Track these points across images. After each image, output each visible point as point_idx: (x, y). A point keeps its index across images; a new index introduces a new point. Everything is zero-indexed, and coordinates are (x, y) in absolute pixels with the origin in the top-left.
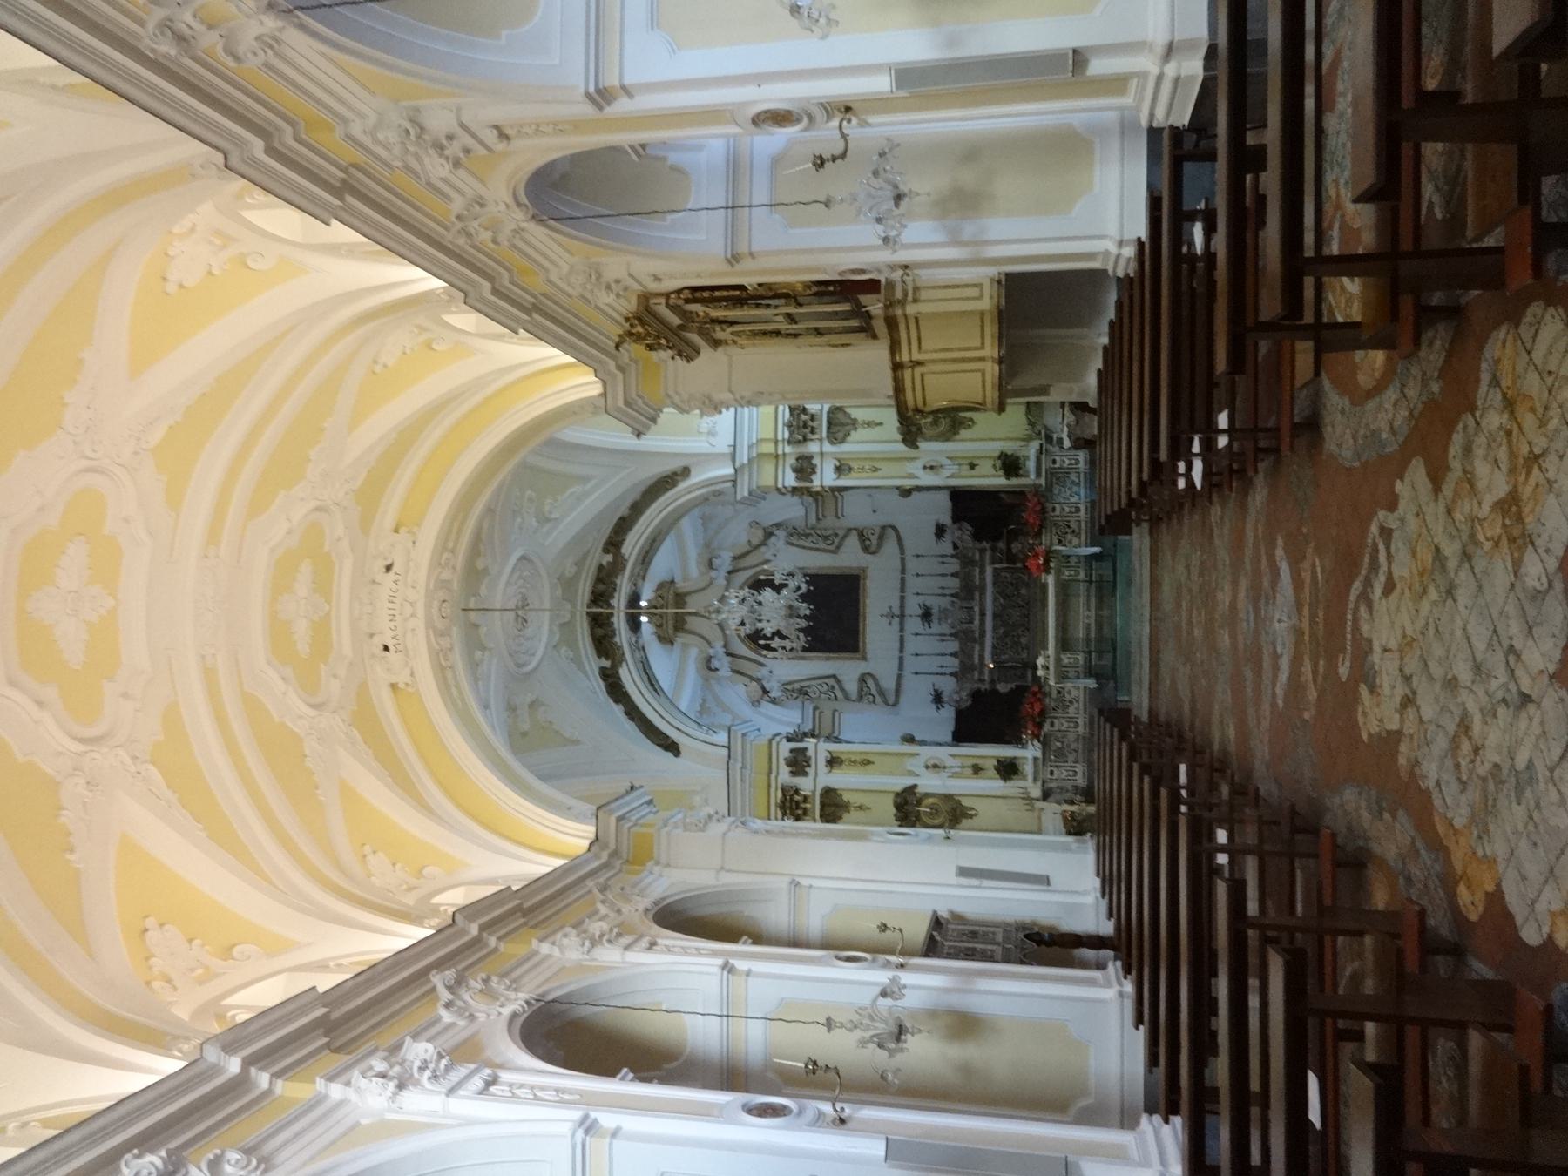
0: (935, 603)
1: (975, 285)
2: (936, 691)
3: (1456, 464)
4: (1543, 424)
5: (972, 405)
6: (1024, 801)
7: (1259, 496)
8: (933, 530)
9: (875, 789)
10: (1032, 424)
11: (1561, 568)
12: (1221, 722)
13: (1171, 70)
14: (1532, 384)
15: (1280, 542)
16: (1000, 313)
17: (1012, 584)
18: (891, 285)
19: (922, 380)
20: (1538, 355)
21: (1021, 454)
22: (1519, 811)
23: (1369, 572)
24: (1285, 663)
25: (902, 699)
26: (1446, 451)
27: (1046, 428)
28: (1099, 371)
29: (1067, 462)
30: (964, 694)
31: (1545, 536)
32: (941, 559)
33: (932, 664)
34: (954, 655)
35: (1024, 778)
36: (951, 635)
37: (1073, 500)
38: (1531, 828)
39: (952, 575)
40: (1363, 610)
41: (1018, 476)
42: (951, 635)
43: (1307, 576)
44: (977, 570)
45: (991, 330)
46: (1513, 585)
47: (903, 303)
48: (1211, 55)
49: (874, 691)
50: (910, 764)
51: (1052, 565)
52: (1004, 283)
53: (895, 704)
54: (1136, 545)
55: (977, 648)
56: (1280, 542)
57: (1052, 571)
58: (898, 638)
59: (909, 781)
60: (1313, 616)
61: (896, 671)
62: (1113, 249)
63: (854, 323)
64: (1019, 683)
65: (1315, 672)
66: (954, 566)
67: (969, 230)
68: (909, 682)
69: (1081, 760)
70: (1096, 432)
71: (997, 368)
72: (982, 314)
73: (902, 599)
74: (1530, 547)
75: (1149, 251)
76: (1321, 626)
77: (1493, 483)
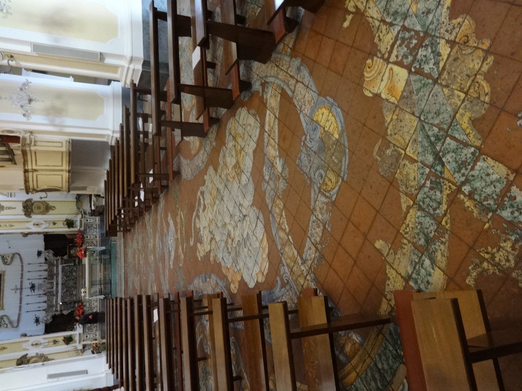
0: (36, 282)
1: (60, 142)
2: (36, 318)
3: (221, 162)
4: (243, 139)
5: (57, 188)
6: (75, 352)
7: (162, 203)
8: (37, 253)
9: (57, 141)
10: (78, 208)
11: (251, 174)
12: (151, 286)
13: (132, 66)
14: (240, 130)
15: (169, 214)
16: (69, 152)
17: (70, 272)
18: (24, 139)
19: (37, 177)
20: (240, 123)
21: (74, 219)
22: (246, 250)
23: (198, 207)
24: (173, 253)
25: (20, 324)
26: (218, 159)
27: (84, 210)
28: (105, 181)
29: (92, 220)
30: (49, 317)
31: (246, 168)
32: (40, 265)
33: (35, 307)
34: (45, 302)
35: (75, 342)
36: (43, 294)
37: (94, 233)
38: (249, 252)
39: (44, 270)
40: (197, 220)
41: (73, 227)
42: (43, 294)
43: (178, 220)
44: (55, 268)
45: (66, 159)
46: (239, 187)
47: (30, 145)
48: (146, 63)
49: (7, 322)
50: (24, 346)
51: (87, 253)
52: (71, 142)
53: (17, 326)
54: (118, 243)
55: (55, 298)
56: (169, 214)
57: (87, 256)
58: (19, 299)
59: (24, 353)
60: (181, 233)
61: (18, 312)
62: (111, 133)
63: (7, 157)
64: (72, 310)
65: (183, 249)
66: (46, 267)
67: (58, 121)
68: (24, 315)
69: (98, 329)
70: (104, 204)
71: (67, 174)
72: (62, 153)
73: (22, 282)
74: (243, 173)
75: (125, 129)
76: (184, 233)
77: (231, 161)
